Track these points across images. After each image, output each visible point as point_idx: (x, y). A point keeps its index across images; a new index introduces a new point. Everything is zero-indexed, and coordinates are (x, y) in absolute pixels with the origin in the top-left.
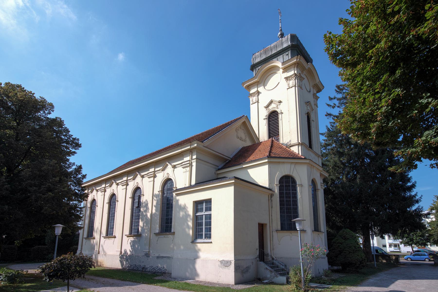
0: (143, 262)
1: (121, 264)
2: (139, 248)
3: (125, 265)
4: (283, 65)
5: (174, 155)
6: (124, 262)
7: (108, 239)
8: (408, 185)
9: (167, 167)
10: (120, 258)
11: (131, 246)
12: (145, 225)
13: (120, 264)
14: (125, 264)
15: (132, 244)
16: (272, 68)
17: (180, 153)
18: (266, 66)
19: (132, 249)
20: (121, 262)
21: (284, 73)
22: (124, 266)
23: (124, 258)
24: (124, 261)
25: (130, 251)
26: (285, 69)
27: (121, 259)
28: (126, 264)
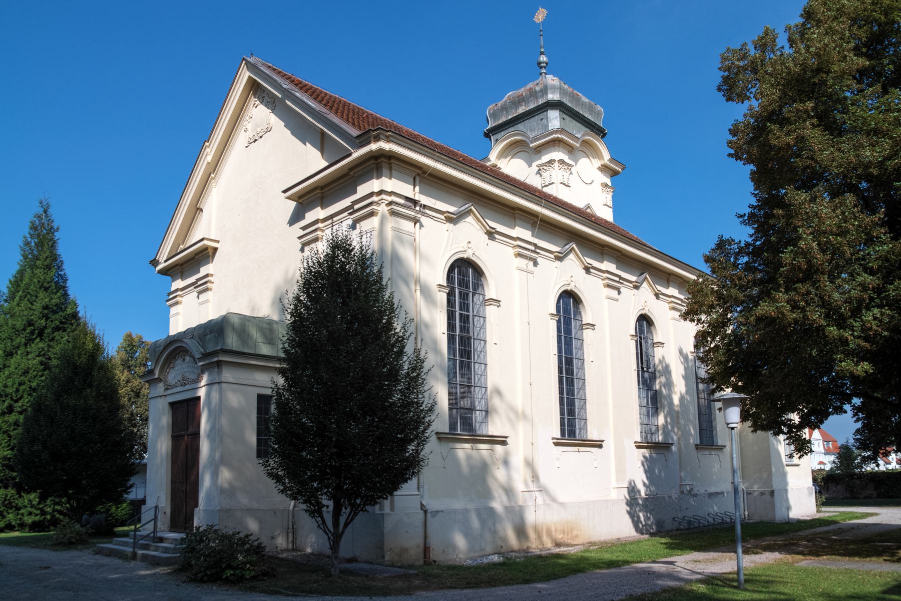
0: (687, 509)
1: (633, 521)
2: (663, 474)
3: (644, 523)
4: (610, 162)
5: (406, 159)
6: (641, 515)
7: (576, 449)
8: (284, 356)
9: (466, 220)
10: (627, 504)
11: (646, 472)
12: (669, 420)
13: (627, 520)
14: (645, 520)
15: (646, 466)
16: (588, 144)
17: (603, 243)
18: (593, 137)
19: (647, 478)
20: (632, 515)
21: (599, 170)
22: (641, 526)
23: (638, 504)
24: (640, 511)
25: (644, 484)
26: (605, 166)
27: (631, 509)
28: (647, 518)
